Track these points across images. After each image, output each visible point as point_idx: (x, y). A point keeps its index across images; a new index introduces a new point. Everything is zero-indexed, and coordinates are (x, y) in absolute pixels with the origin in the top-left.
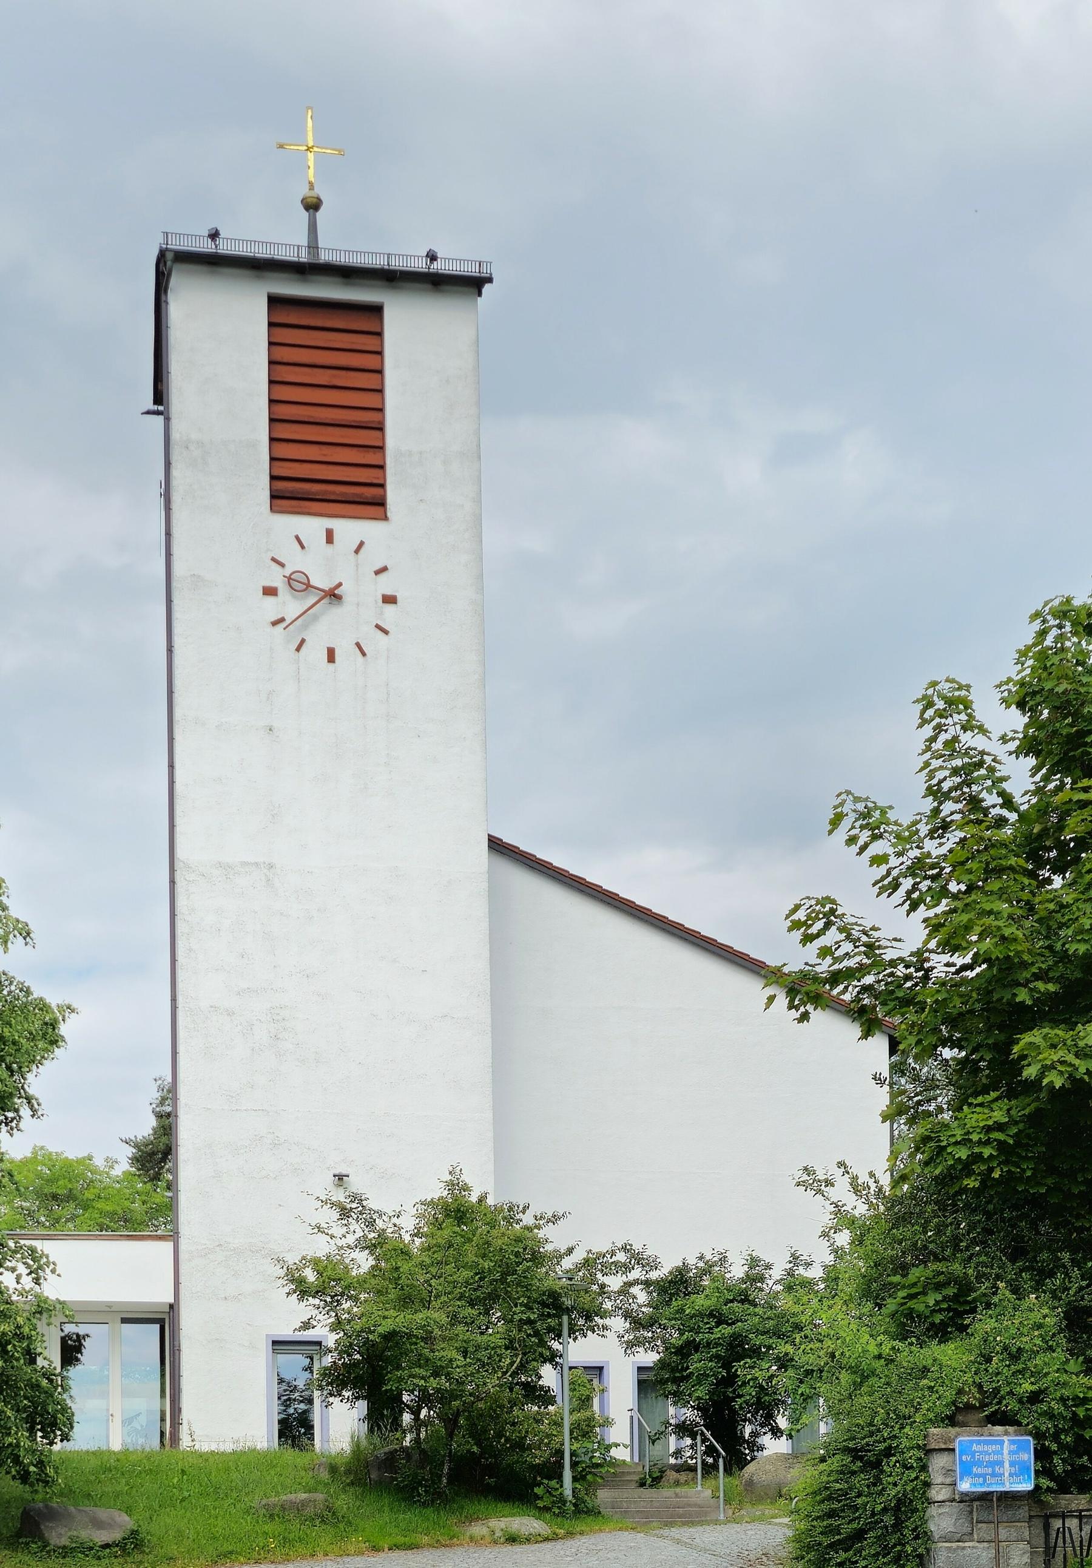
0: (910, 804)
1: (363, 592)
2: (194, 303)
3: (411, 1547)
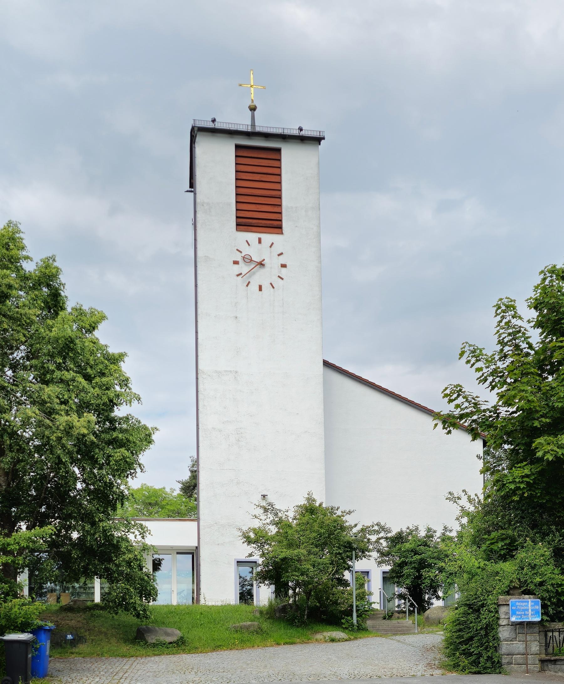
0: (491, 347)
2: (206, 148)
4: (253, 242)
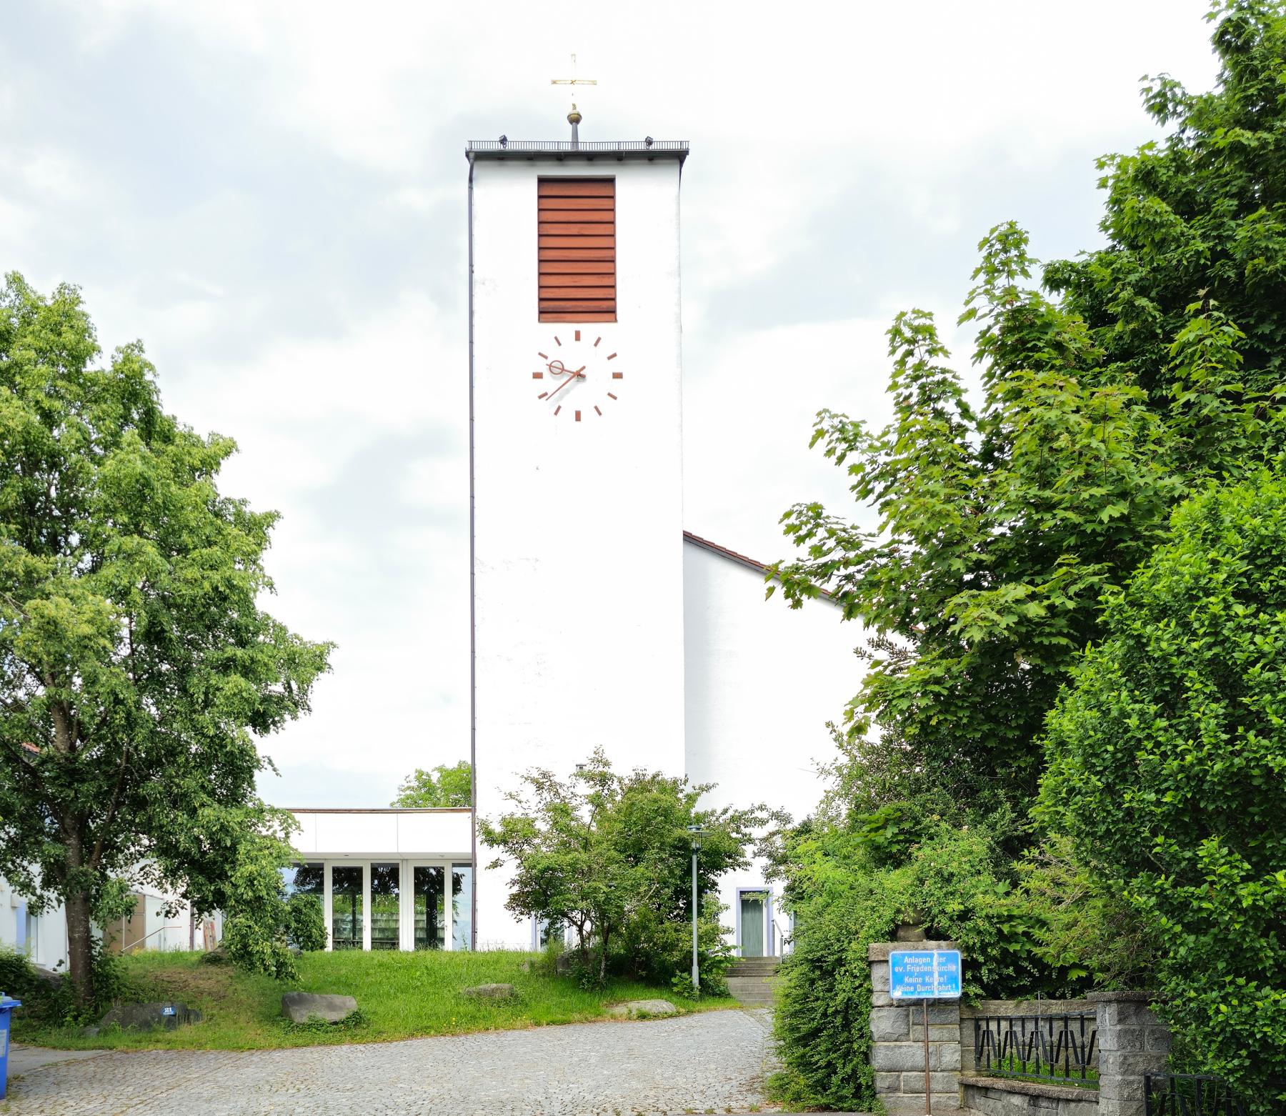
0: (879, 416)
1: (599, 373)
3: (563, 1023)
4: (574, 341)
